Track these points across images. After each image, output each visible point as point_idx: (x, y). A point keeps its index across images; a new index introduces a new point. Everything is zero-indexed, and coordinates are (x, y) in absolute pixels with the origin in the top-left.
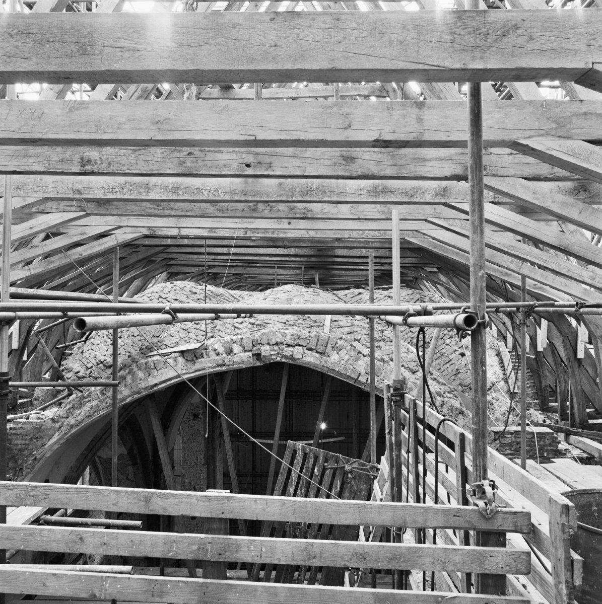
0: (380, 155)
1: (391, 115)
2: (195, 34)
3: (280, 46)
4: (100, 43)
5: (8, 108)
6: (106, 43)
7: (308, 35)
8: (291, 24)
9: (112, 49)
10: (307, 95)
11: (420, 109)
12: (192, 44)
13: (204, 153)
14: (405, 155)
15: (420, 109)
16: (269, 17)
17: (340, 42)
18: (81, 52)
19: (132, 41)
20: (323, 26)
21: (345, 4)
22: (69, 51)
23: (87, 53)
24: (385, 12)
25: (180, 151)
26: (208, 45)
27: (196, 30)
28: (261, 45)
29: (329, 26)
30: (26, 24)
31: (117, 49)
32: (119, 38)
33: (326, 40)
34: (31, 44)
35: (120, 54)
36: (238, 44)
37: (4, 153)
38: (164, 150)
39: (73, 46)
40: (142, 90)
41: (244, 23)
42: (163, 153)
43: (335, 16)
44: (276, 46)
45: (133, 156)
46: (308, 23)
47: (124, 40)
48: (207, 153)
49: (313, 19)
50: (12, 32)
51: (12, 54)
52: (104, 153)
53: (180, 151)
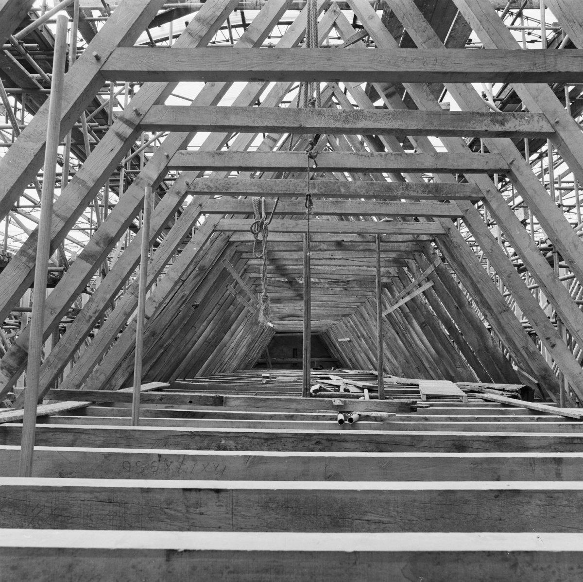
0: (488, 444)
1: (534, 470)
2: (431, 509)
3: (504, 520)
4: (350, 516)
5: (194, 463)
6: (356, 517)
7: (527, 510)
8: (513, 500)
9: (360, 521)
10: (341, 257)
11: (559, 465)
12: (429, 518)
13: (331, 442)
14: (510, 444)
15: (559, 465)
16: (494, 495)
17: (554, 517)
18: (333, 523)
19: (378, 514)
20: (539, 502)
21: (349, 138)
22: (322, 523)
23: (339, 525)
24: (518, 367)
25: (309, 440)
26: (443, 519)
27: (432, 506)
28: (488, 518)
29: (544, 503)
30: (285, 499)
31: (365, 522)
32: (367, 512)
33: (543, 515)
34: (289, 517)
35: (368, 526)
36: (469, 518)
37: (146, 441)
38: (294, 439)
39: (326, 518)
40: (199, 269)
41: (473, 500)
42: (293, 442)
43: (548, 494)
44: (500, 520)
45: (266, 445)
46: (527, 500)
47: (370, 514)
48: (334, 442)
49: (531, 497)
50: (273, 506)
51: (273, 526)
52: (239, 442)
53: (309, 440)
